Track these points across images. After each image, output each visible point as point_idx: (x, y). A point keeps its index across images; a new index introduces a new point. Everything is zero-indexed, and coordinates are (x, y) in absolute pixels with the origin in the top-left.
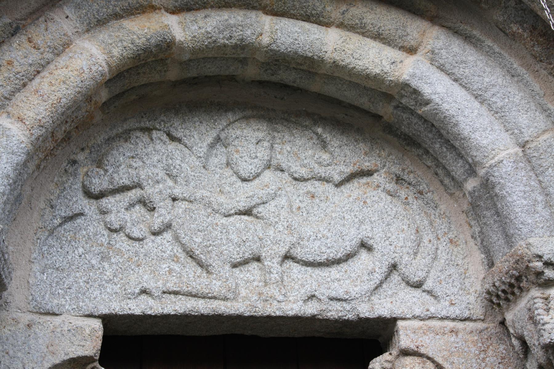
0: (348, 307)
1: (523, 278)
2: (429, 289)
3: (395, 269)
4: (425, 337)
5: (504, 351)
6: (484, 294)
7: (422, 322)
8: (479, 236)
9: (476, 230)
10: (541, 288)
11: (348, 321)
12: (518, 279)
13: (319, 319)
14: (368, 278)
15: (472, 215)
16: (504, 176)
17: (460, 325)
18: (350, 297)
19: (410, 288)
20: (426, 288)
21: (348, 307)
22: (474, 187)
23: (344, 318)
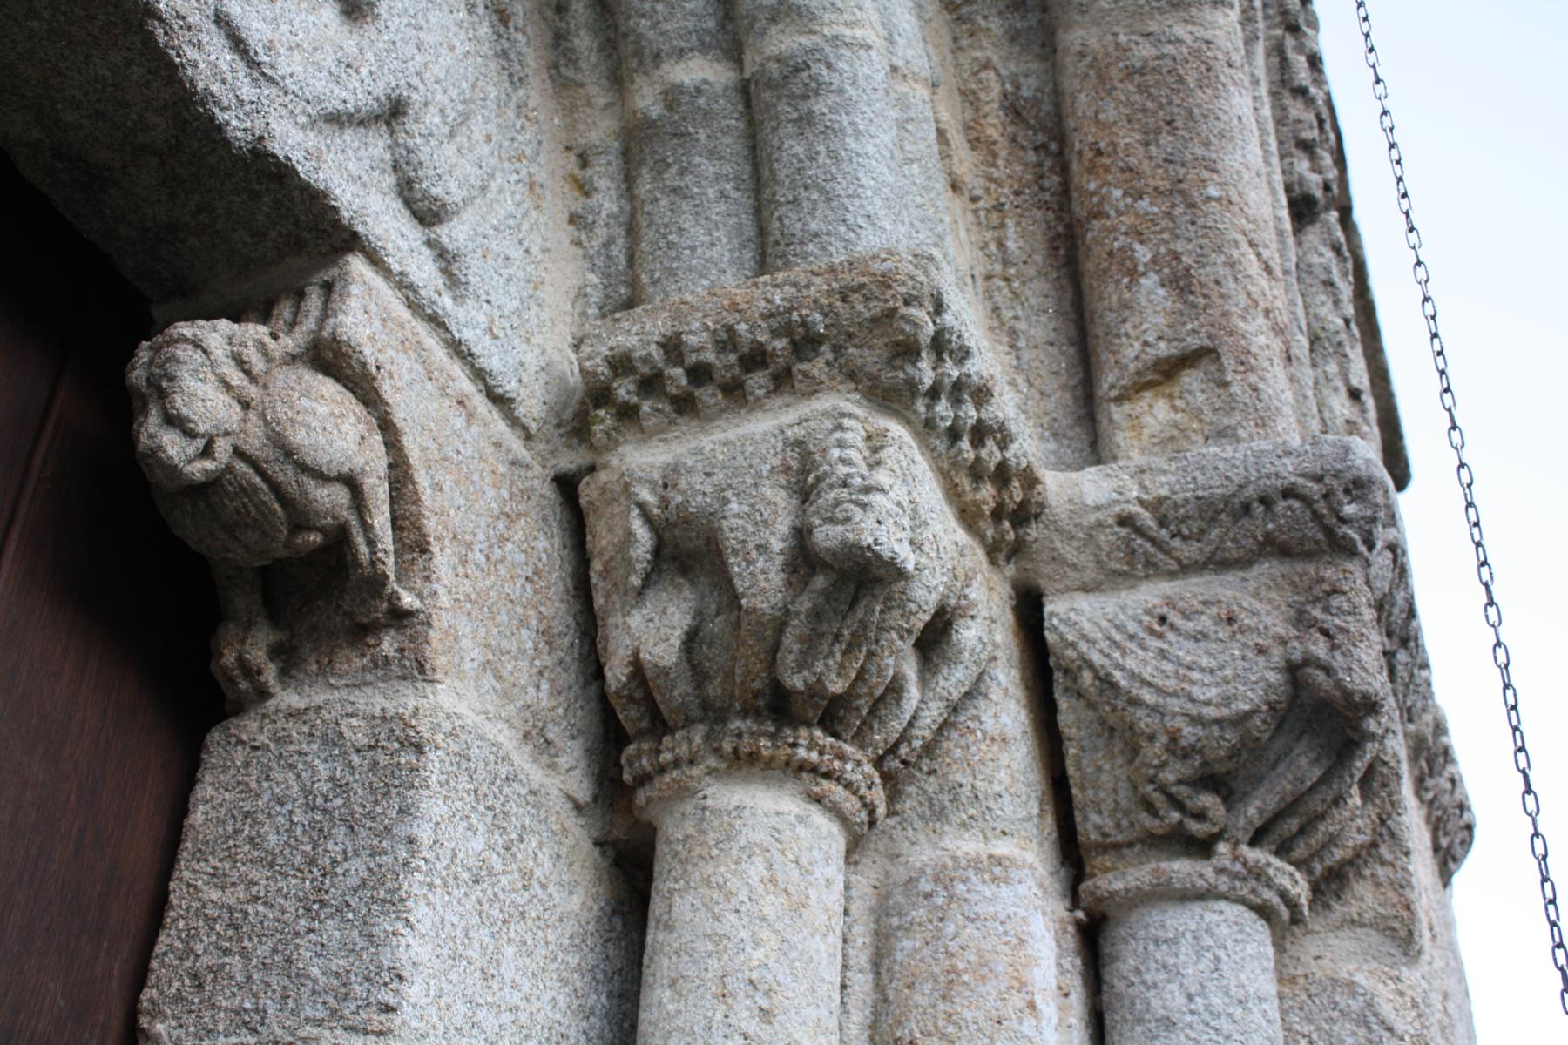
0: (247, 91)
1: (825, 348)
2: (450, 247)
3: (388, 124)
4: (401, 358)
5: (544, 556)
6: (598, 360)
7: (406, 314)
8: (607, 225)
9: (606, 205)
10: (864, 402)
11: (220, 128)
12: (805, 343)
13: (150, 36)
14: (333, 69)
15: (609, 164)
16: (862, 83)
17: (481, 404)
18: (272, 67)
19: (398, 204)
20: (445, 240)
21: (247, 91)
22: (706, 82)
23: (216, 110)
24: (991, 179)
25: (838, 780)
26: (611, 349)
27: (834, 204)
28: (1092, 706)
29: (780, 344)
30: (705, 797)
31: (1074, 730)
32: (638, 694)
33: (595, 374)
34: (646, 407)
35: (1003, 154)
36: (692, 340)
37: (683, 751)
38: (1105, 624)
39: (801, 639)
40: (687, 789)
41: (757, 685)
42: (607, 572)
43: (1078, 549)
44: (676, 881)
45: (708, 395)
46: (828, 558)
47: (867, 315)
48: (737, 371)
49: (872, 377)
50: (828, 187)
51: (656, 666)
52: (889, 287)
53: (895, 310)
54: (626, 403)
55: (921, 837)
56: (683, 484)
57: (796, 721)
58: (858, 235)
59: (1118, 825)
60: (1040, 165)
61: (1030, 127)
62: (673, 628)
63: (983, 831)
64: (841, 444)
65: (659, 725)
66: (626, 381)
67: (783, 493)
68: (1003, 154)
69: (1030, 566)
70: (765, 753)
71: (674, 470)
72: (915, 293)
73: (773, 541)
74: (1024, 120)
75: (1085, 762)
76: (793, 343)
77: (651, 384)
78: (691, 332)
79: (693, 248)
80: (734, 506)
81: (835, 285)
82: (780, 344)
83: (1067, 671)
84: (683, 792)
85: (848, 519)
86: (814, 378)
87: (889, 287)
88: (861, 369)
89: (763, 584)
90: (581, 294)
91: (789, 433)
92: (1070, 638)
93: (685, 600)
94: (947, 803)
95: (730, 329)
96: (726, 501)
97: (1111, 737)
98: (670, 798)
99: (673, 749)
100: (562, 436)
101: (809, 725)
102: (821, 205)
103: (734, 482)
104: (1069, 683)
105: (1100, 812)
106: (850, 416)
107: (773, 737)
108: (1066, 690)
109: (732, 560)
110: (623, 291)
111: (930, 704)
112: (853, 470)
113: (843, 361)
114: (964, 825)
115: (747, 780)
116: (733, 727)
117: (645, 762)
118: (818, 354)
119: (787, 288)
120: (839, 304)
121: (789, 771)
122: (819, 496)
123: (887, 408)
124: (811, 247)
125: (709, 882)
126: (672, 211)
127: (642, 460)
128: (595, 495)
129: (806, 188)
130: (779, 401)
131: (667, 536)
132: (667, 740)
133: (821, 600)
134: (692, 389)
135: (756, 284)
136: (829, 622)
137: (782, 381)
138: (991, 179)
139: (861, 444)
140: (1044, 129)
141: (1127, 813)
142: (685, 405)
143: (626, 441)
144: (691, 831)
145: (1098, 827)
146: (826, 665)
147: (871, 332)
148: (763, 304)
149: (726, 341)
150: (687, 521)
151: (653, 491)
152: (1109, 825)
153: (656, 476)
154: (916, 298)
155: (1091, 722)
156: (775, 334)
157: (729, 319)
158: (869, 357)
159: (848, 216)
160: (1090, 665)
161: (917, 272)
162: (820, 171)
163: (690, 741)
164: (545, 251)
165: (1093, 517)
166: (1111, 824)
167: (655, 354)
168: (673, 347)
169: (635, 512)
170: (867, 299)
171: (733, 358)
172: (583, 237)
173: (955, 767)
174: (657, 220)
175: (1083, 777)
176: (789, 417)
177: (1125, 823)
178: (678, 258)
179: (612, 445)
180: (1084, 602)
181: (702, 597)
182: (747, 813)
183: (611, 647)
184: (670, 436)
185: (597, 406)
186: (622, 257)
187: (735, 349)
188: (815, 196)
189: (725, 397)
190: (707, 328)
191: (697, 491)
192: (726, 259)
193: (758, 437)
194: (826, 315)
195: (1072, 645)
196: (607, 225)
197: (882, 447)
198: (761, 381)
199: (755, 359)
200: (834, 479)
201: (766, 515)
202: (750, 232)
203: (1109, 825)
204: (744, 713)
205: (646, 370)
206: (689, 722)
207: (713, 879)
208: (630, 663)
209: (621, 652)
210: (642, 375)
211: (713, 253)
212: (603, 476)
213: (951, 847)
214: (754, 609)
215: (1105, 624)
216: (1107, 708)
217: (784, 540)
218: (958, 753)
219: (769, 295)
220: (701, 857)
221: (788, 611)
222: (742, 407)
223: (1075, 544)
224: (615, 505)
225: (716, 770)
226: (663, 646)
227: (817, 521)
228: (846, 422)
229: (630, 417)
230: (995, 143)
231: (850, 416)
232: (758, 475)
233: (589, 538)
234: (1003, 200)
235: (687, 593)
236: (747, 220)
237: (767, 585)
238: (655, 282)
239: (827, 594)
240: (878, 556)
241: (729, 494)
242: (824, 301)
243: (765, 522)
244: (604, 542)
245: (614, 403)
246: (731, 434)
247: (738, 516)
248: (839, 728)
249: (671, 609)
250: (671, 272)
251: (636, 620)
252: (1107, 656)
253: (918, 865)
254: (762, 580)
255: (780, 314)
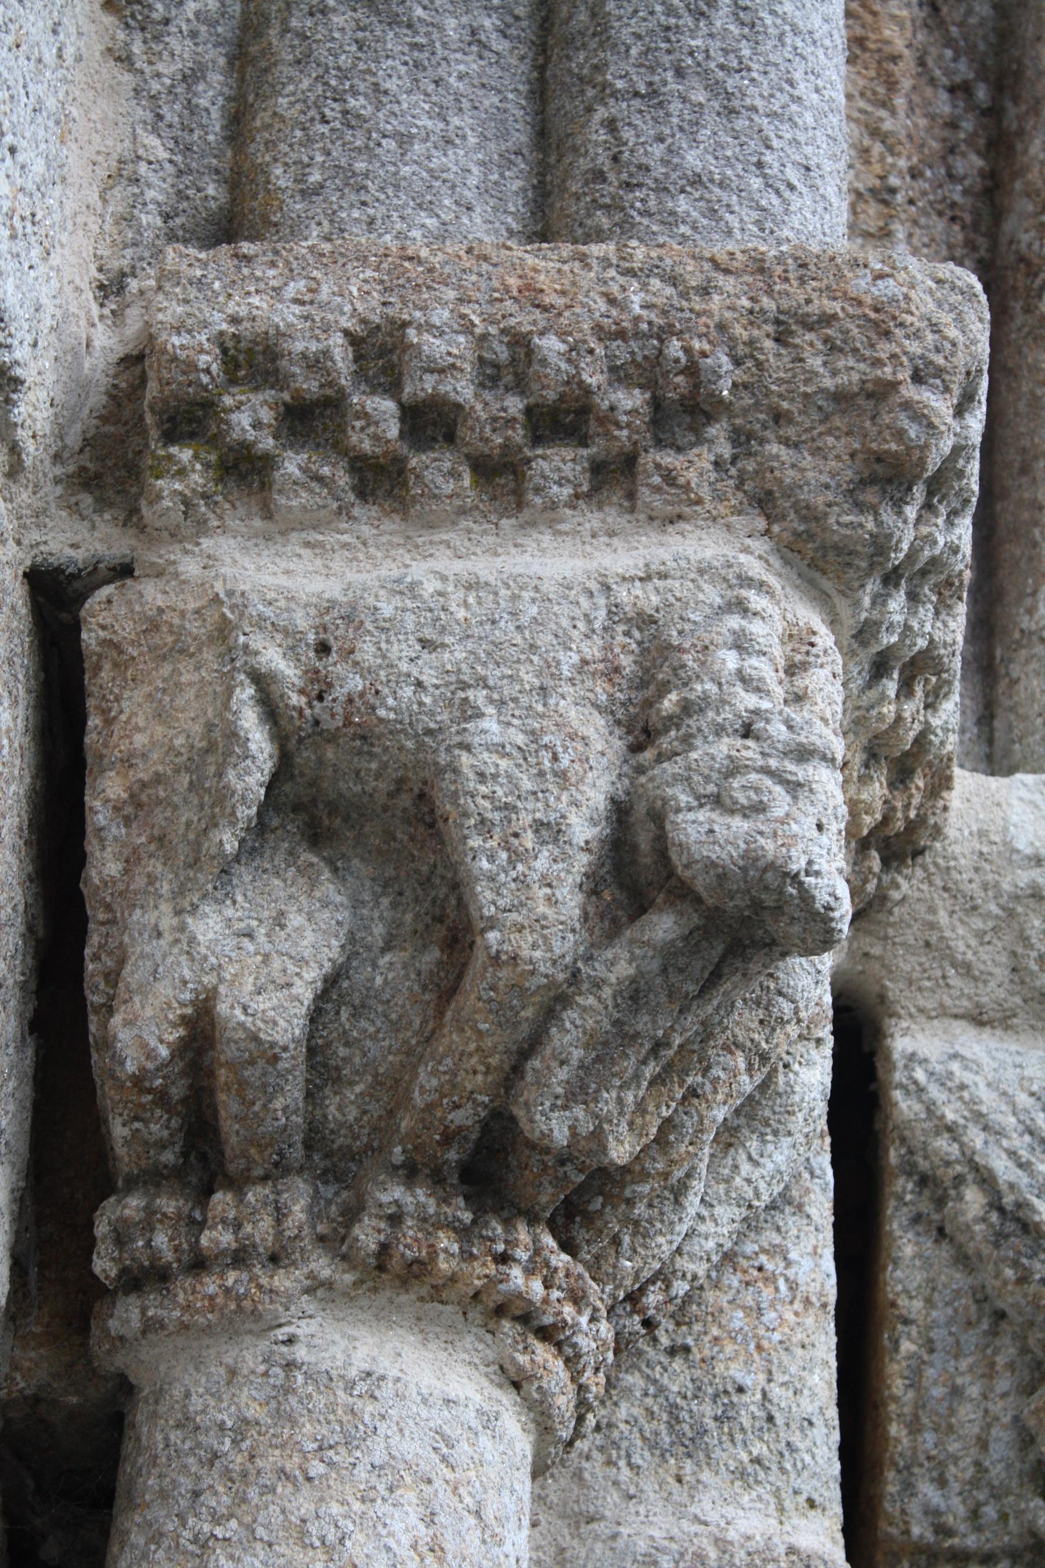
1: (717, 430)
12: (682, 409)
24: (875, 133)
25: (559, 1345)
26: (234, 320)
27: (741, 123)
28: (963, 1260)
29: (630, 400)
30: (290, 1341)
31: (918, 1304)
32: (177, 1092)
33: (191, 366)
34: (292, 465)
35: (906, 84)
36: (434, 346)
37: (261, 1230)
38: (1023, 1099)
39: (591, 1041)
40: (256, 1315)
41: (460, 1117)
42: (135, 807)
43: (980, 935)
44: (217, 1519)
45: (438, 471)
46: (701, 884)
47: (828, 383)
48: (518, 435)
49: (809, 514)
50: (731, 83)
51: (255, 1038)
52: (887, 334)
53: (894, 386)
54: (246, 447)
55: (649, 1486)
56: (367, 652)
57: (515, 1209)
58: (786, 202)
59: (975, 1514)
60: (953, 125)
61: (949, 42)
62: (301, 961)
63: (777, 1493)
64: (741, 644)
65: (203, 1161)
66: (257, 398)
67: (600, 721)
68: (906, 84)
69: (876, 951)
70: (444, 1265)
71: (348, 619)
72: (939, 360)
73: (573, 819)
74: (942, 24)
75: (930, 1372)
76: (656, 404)
77: (310, 418)
78: (429, 327)
79: (404, 140)
80: (490, 724)
81: (767, 303)
82: (630, 400)
83: (924, 1181)
84: (245, 1318)
85: (759, 808)
86: (687, 487)
87: (887, 334)
88: (789, 492)
89: (542, 909)
90: (123, 173)
91: (622, 594)
92: (950, 1116)
93: (325, 904)
94: (710, 1424)
95: (521, 344)
96: (469, 713)
97: (994, 1332)
98: (208, 1329)
99: (238, 1226)
100: (57, 481)
101: (533, 1220)
102: (709, 118)
103: (493, 674)
104: (925, 1206)
105: (941, 1482)
106: (761, 586)
107: (464, 1233)
108: (916, 1219)
109: (475, 842)
110: (211, 191)
111: (719, 1210)
112: (765, 705)
113: (750, 466)
114: (741, 1474)
115: (382, 1318)
116: (385, 1198)
117: (161, 1239)
118: (700, 441)
119: (655, 283)
120: (769, 344)
121: (475, 1314)
122: (687, 741)
123: (812, 583)
124: (683, 204)
125: (303, 1533)
126: (360, 45)
127: (279, 578)
128: (126, 630)
129: (680, 73)
130: (593, 520)
131: (305, 757)
132: (222, 1200)
133: (655, 965)
134: (403, 449)
135: (583, 258)
136: (654, 1013)
137: (614, 477)
138: (875, 133)
139: (777, 651)
140: (971, 50)
141: (997, 1494)
142: (380, 482)
143: (224, 529)
144: (255, 1411)
145: (932, 1513)
146: (620, 1101)
147: (826, 418)
148: (602, 305)
149: (510, 363)
150: (364, 734)
151: (291, 652)
152: (955, 1512)
153: (302, 621)
154: (939, 372)
155: (957, 1294)
156: (619, 375)
157: (524, 320)
158: (814, 472)
159: (768, 158)
160: (986, 1179)
161: (945, 318)
162: (715, 45)
163: (280, 1215)
164: (79, 59)
165: (1024, 877)
166: (961, 1510)
167: (338, 354)
168: (381, 352)
169: (246, 692)
170: (832, 348)
171: (515, 405)
172: (137, 48)
173: (729, 1348)
174: (321, 53)
175: (920, 1405)
176: (622, 558)
177: (990, 1512)
178: (368, 151)
179: (188, 528)
180: (977, 1045)
181: (356, 904)
182: (386, 1391)
183: (134, 974)
184: (330, 539)
185: (170, 437)
186: (215, 114)
187: (520, 386)
188: (700, 96)
189: (476, 484)
190: (468, 328)
191: (400, 676)
192: (472, 181)
193: (548, 588)
194: (737, 362)
195: (951, 1129)
196: (194, 34)
197: (805, 666)
198: (567, 469)
199: (563, 419)
200: (727, 714)
201: (565, 762)
202: (521, 136)
203: (955, 1512)
204: (410, 1173)
205: (310, 386)
206: (279, 1170)
207: (313, 1528)
208: (184, 1020)
209: (164, 990)
210: (297, 394)
211: (450, 160)
212: (152, 594)
213: (712, 1517)
214: (515, 958)
215: (1023, 1099)
216: (1009, 1273)
217: (593, 822)
218: (738, 1319)
219: (615, 289)
220: (282, 1473)
221: (576, 974)
222: (505, 513)
223: (977, 923)
224: (185, 665)
225: (329, 1285)
226: (277, 997)
227: (684, 799)
228: (756, 601)
229: (242, 477)
230: (895, 58)
231: (761, 586)
232: (551, 668)
233: (94, 721)
234: (894, 181)
235: (328, 888)
236: (517, 109)
237: (549, 912)
238: (308, 193)
239: (670, 958)
240: (806, 897)
241: (478, 696)
242: (738, 331)
243: (562, 775)
244: (140, 740)
245: (214, 441)
246: (484, 567)
247: (500, 750)
248: (581, 1235)
249: (295, 920)
250: (353, 182)
251: (209, 927)
252: (1024, 1166)
253: (642, 1546)
254: (535, 899)
255: (638, 335)
